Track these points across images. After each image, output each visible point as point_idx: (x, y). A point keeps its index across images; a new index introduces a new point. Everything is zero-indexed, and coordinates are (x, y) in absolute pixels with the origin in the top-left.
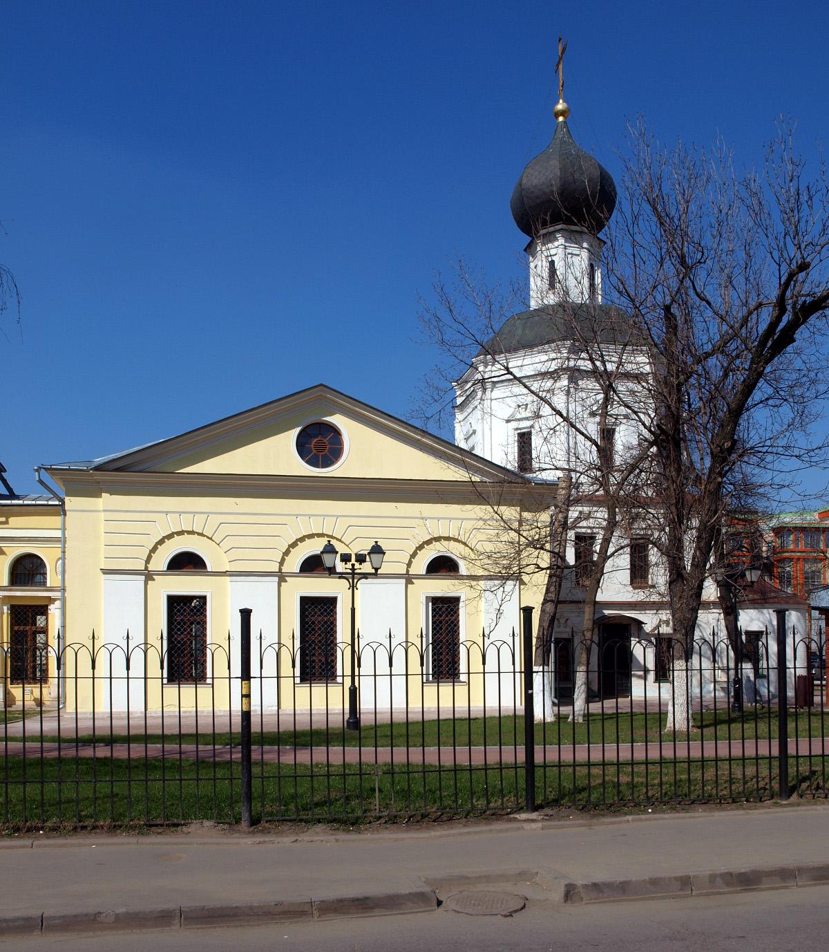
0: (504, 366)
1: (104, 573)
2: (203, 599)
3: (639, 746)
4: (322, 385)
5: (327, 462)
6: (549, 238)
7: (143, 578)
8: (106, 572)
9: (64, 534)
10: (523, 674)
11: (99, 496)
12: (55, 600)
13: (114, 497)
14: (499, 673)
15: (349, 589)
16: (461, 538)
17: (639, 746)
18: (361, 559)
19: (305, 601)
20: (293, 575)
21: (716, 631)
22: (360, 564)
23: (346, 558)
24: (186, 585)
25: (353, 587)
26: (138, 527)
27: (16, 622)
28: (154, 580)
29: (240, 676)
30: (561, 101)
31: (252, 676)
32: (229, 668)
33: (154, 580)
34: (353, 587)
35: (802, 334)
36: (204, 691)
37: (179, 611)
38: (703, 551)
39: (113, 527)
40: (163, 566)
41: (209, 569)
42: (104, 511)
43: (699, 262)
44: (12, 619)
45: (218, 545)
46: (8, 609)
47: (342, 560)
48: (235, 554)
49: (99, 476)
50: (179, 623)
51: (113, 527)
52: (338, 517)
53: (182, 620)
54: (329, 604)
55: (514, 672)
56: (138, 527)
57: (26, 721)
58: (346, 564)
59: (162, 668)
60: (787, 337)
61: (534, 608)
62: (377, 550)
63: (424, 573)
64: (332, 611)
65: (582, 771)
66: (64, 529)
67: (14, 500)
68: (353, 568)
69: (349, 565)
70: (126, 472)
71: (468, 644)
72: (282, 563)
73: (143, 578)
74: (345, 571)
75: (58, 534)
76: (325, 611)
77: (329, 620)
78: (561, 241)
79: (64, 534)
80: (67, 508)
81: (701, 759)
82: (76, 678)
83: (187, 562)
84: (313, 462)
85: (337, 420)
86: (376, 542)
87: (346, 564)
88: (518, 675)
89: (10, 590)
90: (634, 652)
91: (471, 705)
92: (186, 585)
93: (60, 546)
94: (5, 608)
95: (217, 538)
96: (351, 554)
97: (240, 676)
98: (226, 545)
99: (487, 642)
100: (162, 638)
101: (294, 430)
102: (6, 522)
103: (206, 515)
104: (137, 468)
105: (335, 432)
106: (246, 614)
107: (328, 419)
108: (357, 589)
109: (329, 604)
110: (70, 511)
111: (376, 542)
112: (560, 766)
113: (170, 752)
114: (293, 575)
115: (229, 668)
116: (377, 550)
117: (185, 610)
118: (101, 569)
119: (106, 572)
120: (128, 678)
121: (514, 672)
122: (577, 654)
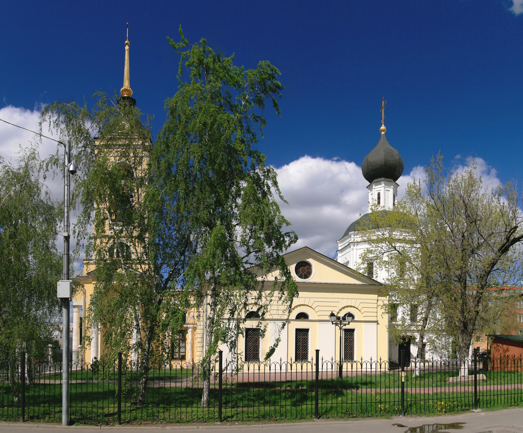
2: (296, 329)
4: (306, 247)
5: (306, 277)
6: (378, 183)
12: (189, 328)
16: (359, 308)
19: (297, 330)
20: (293, 320)
24: (302, 325)
30: (383, 125)
36: (305, 365)
41: (310, 318)
43: (467, 211)
48: (320, 313)
52: (310, 298)
64: (307, 334)
76: (254, 334)
78: (383, 185)
84: (300, 277)
85: (310, 260)
90: (411, 351)
92: (302, 325)
95: (317, 310)
105: (309, 265)
107: (307, 260)
109: (306, 331)
113: (47, 410)
114: (293, 320)
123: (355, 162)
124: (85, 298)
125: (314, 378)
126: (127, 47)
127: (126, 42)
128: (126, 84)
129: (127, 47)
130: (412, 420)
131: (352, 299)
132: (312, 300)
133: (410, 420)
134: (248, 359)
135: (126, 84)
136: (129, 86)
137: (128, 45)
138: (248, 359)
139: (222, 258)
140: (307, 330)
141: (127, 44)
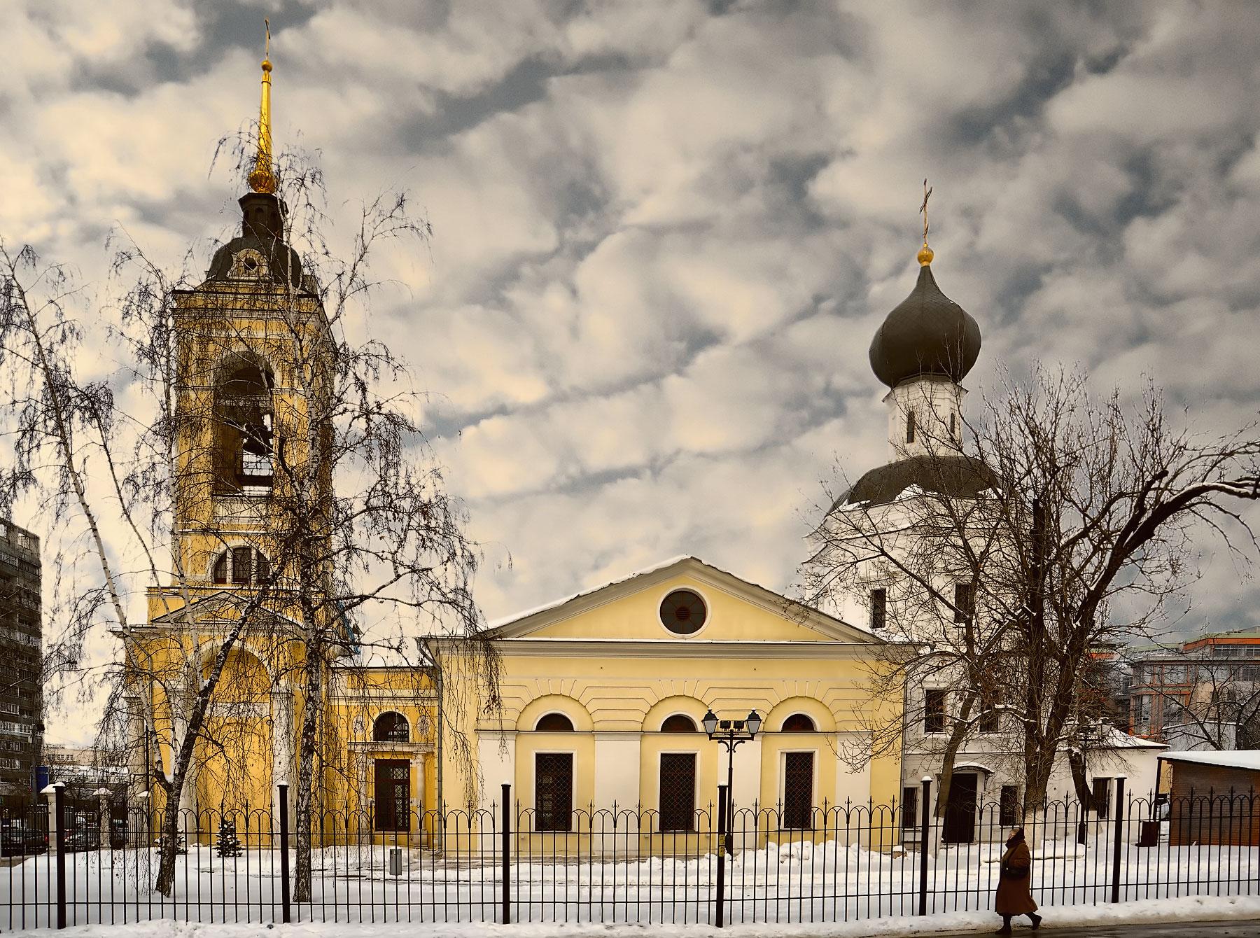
0: (878, 547)
3: (1060, 844)
4: (758, 586)
17: (1060, 844)
19: (540, 757)
25: (731, 750)
32: (494, 827)
34: (731, 750)
35: (1161, 530)
36: (560, 838)
38: (1058, 718)
54: (566, 760)
60: (1146, 533)
62: (754, 717)
71: (579, 812)
83: (555, 723)
92: (554, 744)
109: (566, 760)
115: (494, 827)
116: (754, 717)
121: (756, 832)
134: (541, 826)
138: (541, 826)
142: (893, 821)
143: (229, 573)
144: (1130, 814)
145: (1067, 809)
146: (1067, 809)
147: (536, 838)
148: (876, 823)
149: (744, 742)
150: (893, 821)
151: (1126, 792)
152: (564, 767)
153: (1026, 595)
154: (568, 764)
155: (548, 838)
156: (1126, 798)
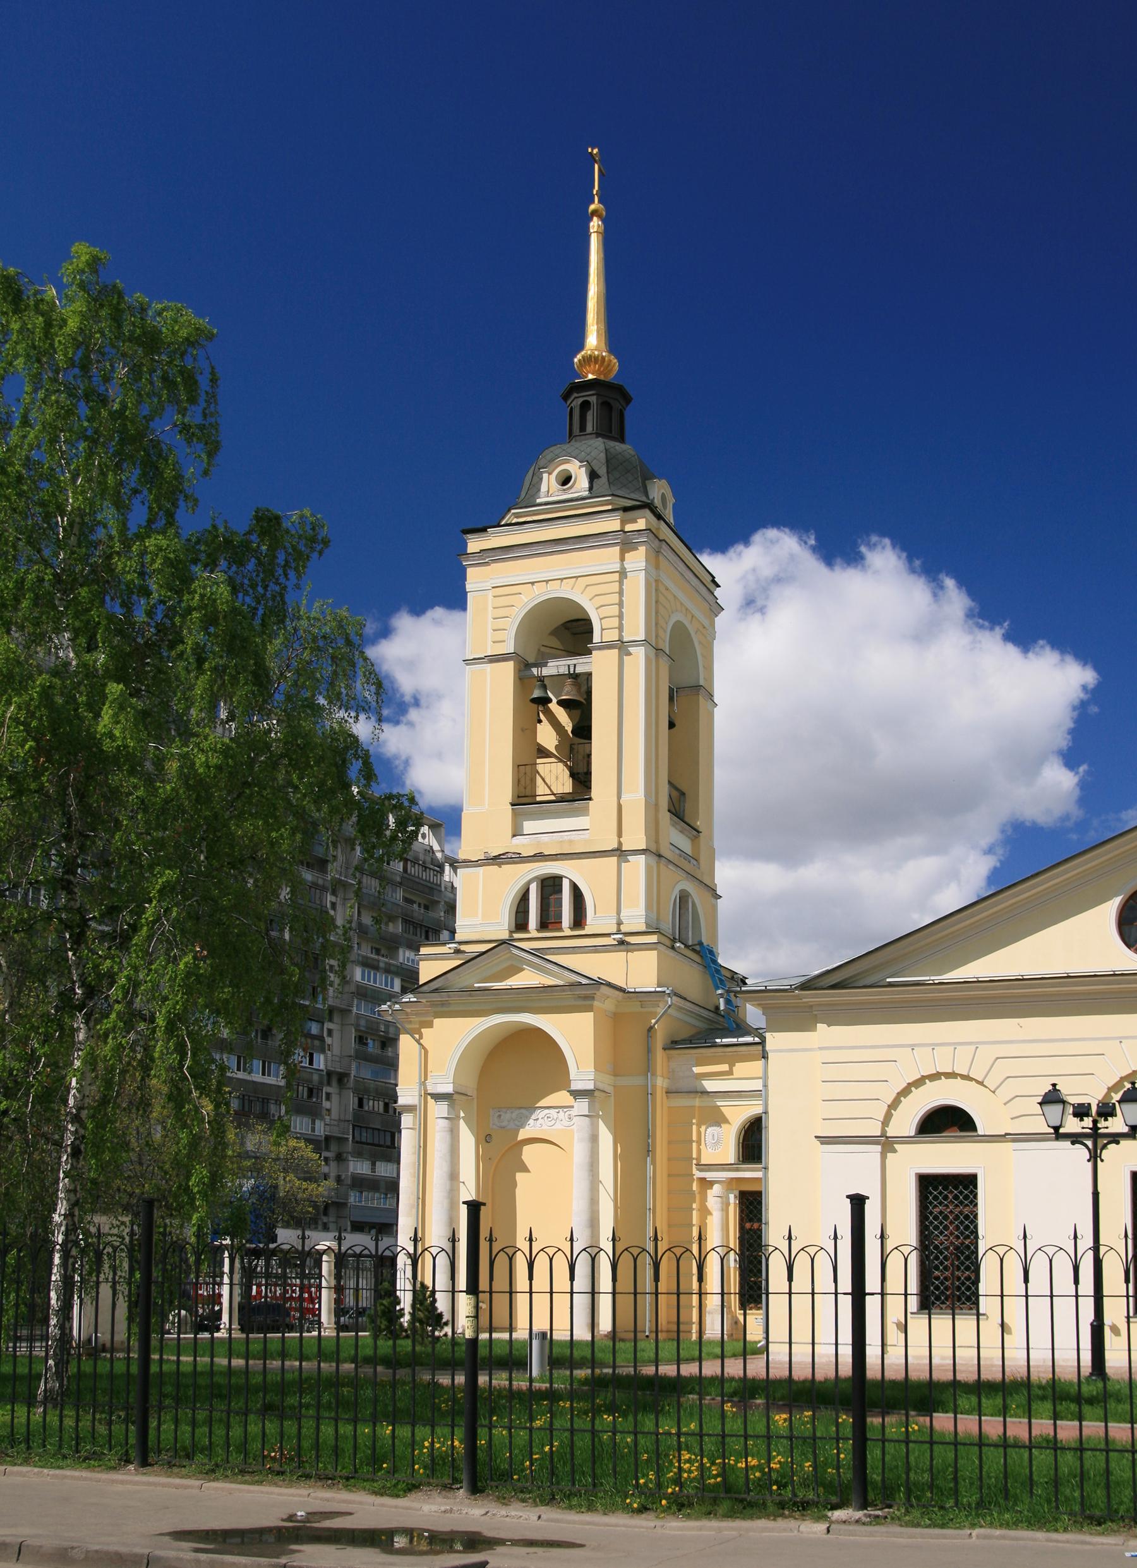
1: (822, 1143)
7: (878, 1148)
8: (825, 1140)
9: (765, 1086)
10: (1131, 1299)
11: (812, 1028)
13: (833, 1028)
14: (1052, 1296)
15: (1089, 1161)
18: (1106, 1111)
19: (928, 1184)
21: (420, 1235)
22: (1106, 1120)
23: (1081, 1112)
26: (872, 1071)
27: (747, 1216)
28: (895, 1151)
29: (867, 1297)
31: (850, 1297)
33: (895, 1151)
34: (1095, 1157)
36: (966, 1324)
37: (936, 1198)
39: (833, 1072)
40: (911, 1130)
41: (980, 1132)
42: (821, 1049)
44: (741, 1211)
45: (994, 1092)
46: (735, 1197)
47: (1075, 1115)
49: (809, 997)
50: (936, 1218)
51: (833, 1072)
53: (941, 1213)
54: (967, 1183)
55: (906, 1295)
56: (872, 1071)
57: (703, 1363)
58: (1082, 1120)
59: (1127, 1281)
61: (868, 1198)
63: (913, 1133)
65: (994, 1458)
66: (765, 1078)
67: (742, 1036)
68: (1095, 1127)
69: (1088, 1122)
70: (815, 989)
72: (886, 1122)
73: (878, 1148)
74: (1080, 1130)
75: (757, 1085)
77: (961, 1212)
79: (765, 1086)
80: (768, 1048)
81: (1129, 1447)
82: (1052, 1296)
86: (1054, 1085)
87: (1082, 1120)
88: (1131, 1299)
89: (737, 1170)
91: (839, 1352)
93: (761, 1102)
94: (732, 1196)
96: (1089, 1104)
97: (867, 1297)
98: (1005, 1093)
99: (536, 1247)
100: (1126, 1236)
101: (1112, 901)
102: (730, 1072)
103: (973, 1047)
104: (861, 984)
106: (858, 1202)
108: (1102, 1161)
109: (967, 1183)
110: (771, 1051)
111: (1054, 1085)
112: (956, 1444)
117: (946, 1198)
118: (816, 1137)
119: (825, 1140)
120: (1027, 1296)
122: (330, 1272)
123: (439, 606)
124: (426, 1079)
125: (846, 1369)
126: (595, 224)
127: (592, 207)
128: (593, 339)
129: (595, 224)
130: (434, 1508)
131: (933, 1046)
132: (986, 1054)
133: (426, 1508)
134: (929, 1300)
135: (593, 339)
136: (603, 346)
137: (599, 217)
138: (929, 1300)
139: (98, 954)
140: (969, 1181)
141: (595, 213)
142: (1076, 1281)
143: (480, 911)
144: (531, 1278)
145: (656, 1266)
146: (656, 1266)
147: (918, 1325)
148: (1038, 1283)
149: (1118, 1143)
150: (1076, 1281)
151: (484, 1233)
152: (967, 1197)
153: (118, 877)
154: (971, 1192)
155: (942, 1323)
156: (484, 1246)
